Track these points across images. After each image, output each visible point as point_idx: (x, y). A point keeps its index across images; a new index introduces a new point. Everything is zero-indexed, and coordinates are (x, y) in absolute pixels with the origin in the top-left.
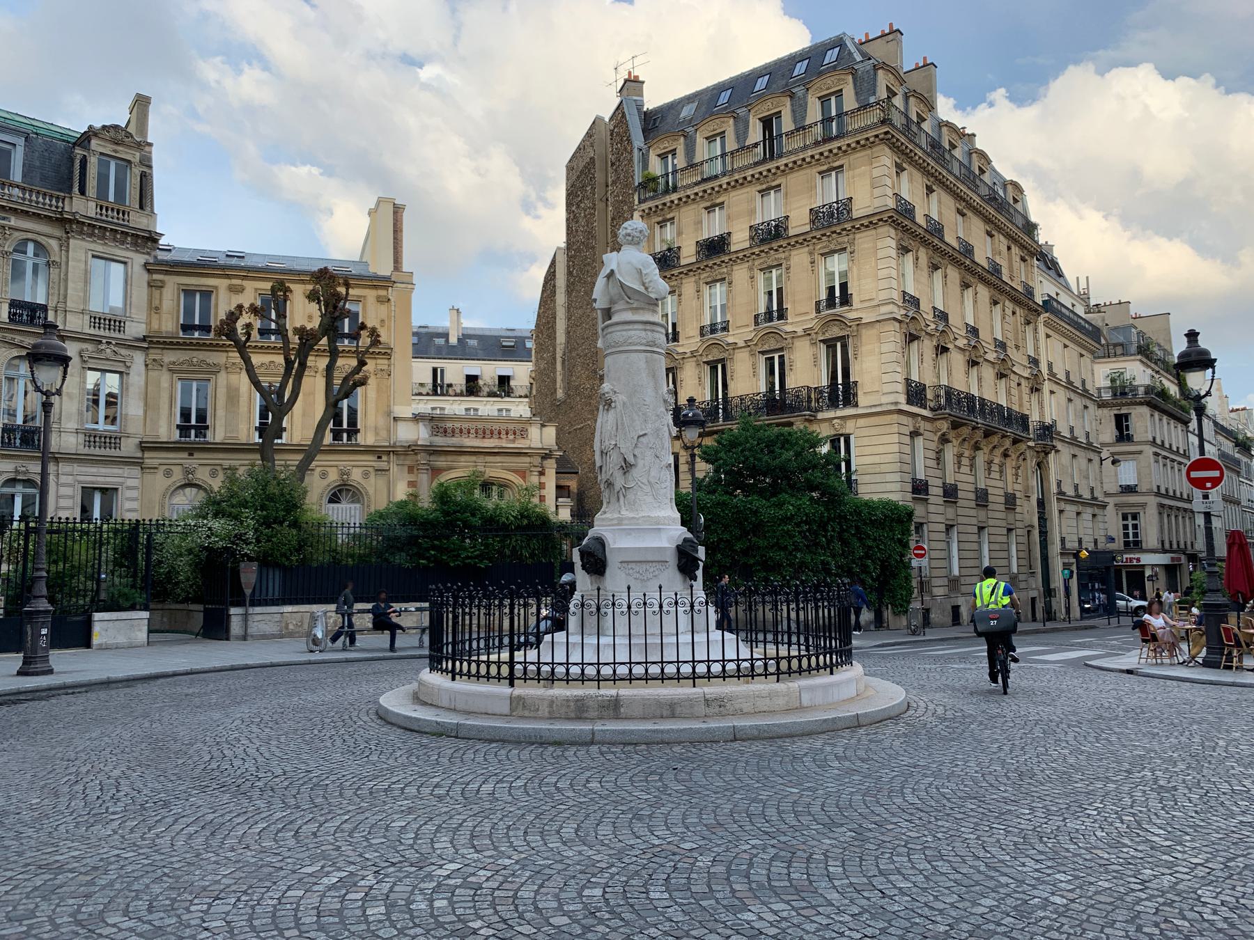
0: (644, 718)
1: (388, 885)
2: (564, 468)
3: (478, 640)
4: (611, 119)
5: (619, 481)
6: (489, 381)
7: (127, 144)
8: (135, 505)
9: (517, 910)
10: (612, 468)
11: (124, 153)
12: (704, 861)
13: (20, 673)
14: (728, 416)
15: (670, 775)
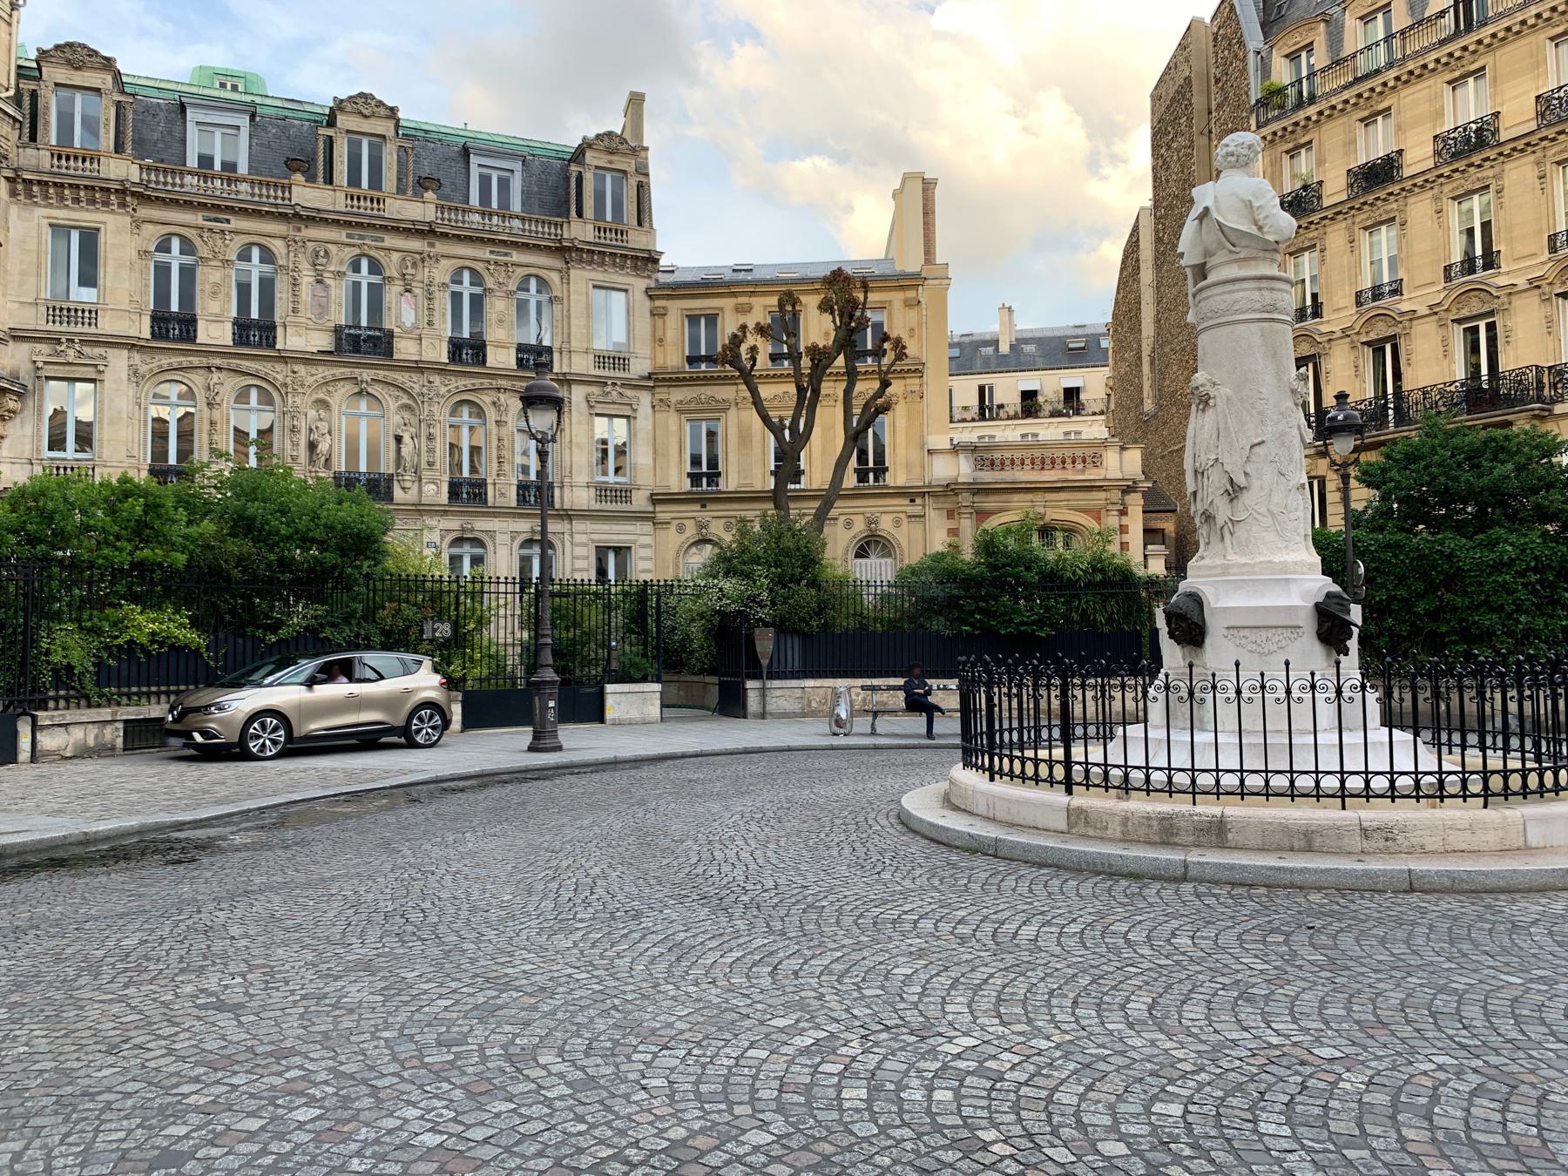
0: (1263, 850)
1: (877, 1058)
2: (1155, 504)
3: (1011, 731)
4: (1214, 17)
5: (1223, 512)
6: (1052, 397)
7: (624, 149)
8: (649, 565)
9: (1049, 1121)
10: (1211, 493)
11: (620, 163)
12: (1353, 1082)
13: (531, 749)
14: (1402, 418)
15: (1302, 937)
